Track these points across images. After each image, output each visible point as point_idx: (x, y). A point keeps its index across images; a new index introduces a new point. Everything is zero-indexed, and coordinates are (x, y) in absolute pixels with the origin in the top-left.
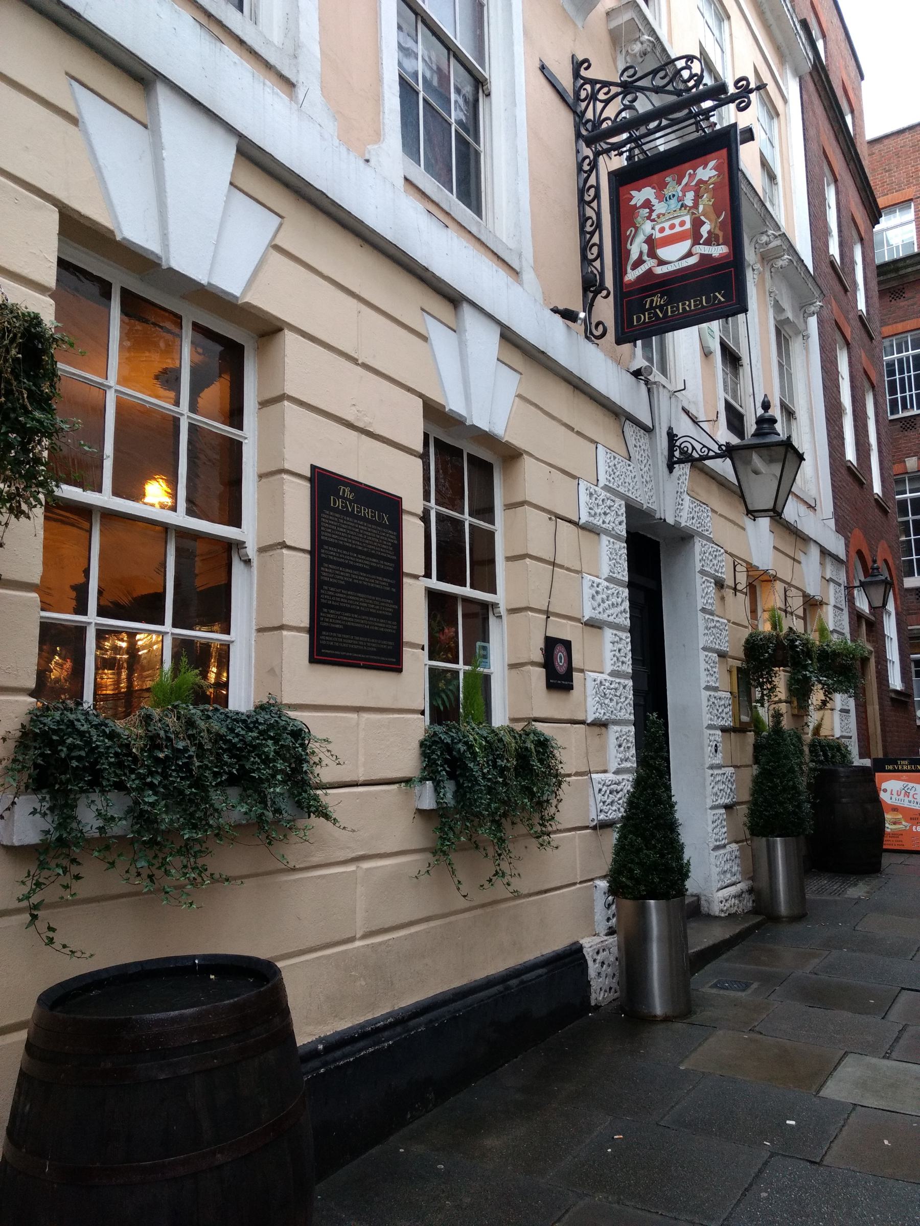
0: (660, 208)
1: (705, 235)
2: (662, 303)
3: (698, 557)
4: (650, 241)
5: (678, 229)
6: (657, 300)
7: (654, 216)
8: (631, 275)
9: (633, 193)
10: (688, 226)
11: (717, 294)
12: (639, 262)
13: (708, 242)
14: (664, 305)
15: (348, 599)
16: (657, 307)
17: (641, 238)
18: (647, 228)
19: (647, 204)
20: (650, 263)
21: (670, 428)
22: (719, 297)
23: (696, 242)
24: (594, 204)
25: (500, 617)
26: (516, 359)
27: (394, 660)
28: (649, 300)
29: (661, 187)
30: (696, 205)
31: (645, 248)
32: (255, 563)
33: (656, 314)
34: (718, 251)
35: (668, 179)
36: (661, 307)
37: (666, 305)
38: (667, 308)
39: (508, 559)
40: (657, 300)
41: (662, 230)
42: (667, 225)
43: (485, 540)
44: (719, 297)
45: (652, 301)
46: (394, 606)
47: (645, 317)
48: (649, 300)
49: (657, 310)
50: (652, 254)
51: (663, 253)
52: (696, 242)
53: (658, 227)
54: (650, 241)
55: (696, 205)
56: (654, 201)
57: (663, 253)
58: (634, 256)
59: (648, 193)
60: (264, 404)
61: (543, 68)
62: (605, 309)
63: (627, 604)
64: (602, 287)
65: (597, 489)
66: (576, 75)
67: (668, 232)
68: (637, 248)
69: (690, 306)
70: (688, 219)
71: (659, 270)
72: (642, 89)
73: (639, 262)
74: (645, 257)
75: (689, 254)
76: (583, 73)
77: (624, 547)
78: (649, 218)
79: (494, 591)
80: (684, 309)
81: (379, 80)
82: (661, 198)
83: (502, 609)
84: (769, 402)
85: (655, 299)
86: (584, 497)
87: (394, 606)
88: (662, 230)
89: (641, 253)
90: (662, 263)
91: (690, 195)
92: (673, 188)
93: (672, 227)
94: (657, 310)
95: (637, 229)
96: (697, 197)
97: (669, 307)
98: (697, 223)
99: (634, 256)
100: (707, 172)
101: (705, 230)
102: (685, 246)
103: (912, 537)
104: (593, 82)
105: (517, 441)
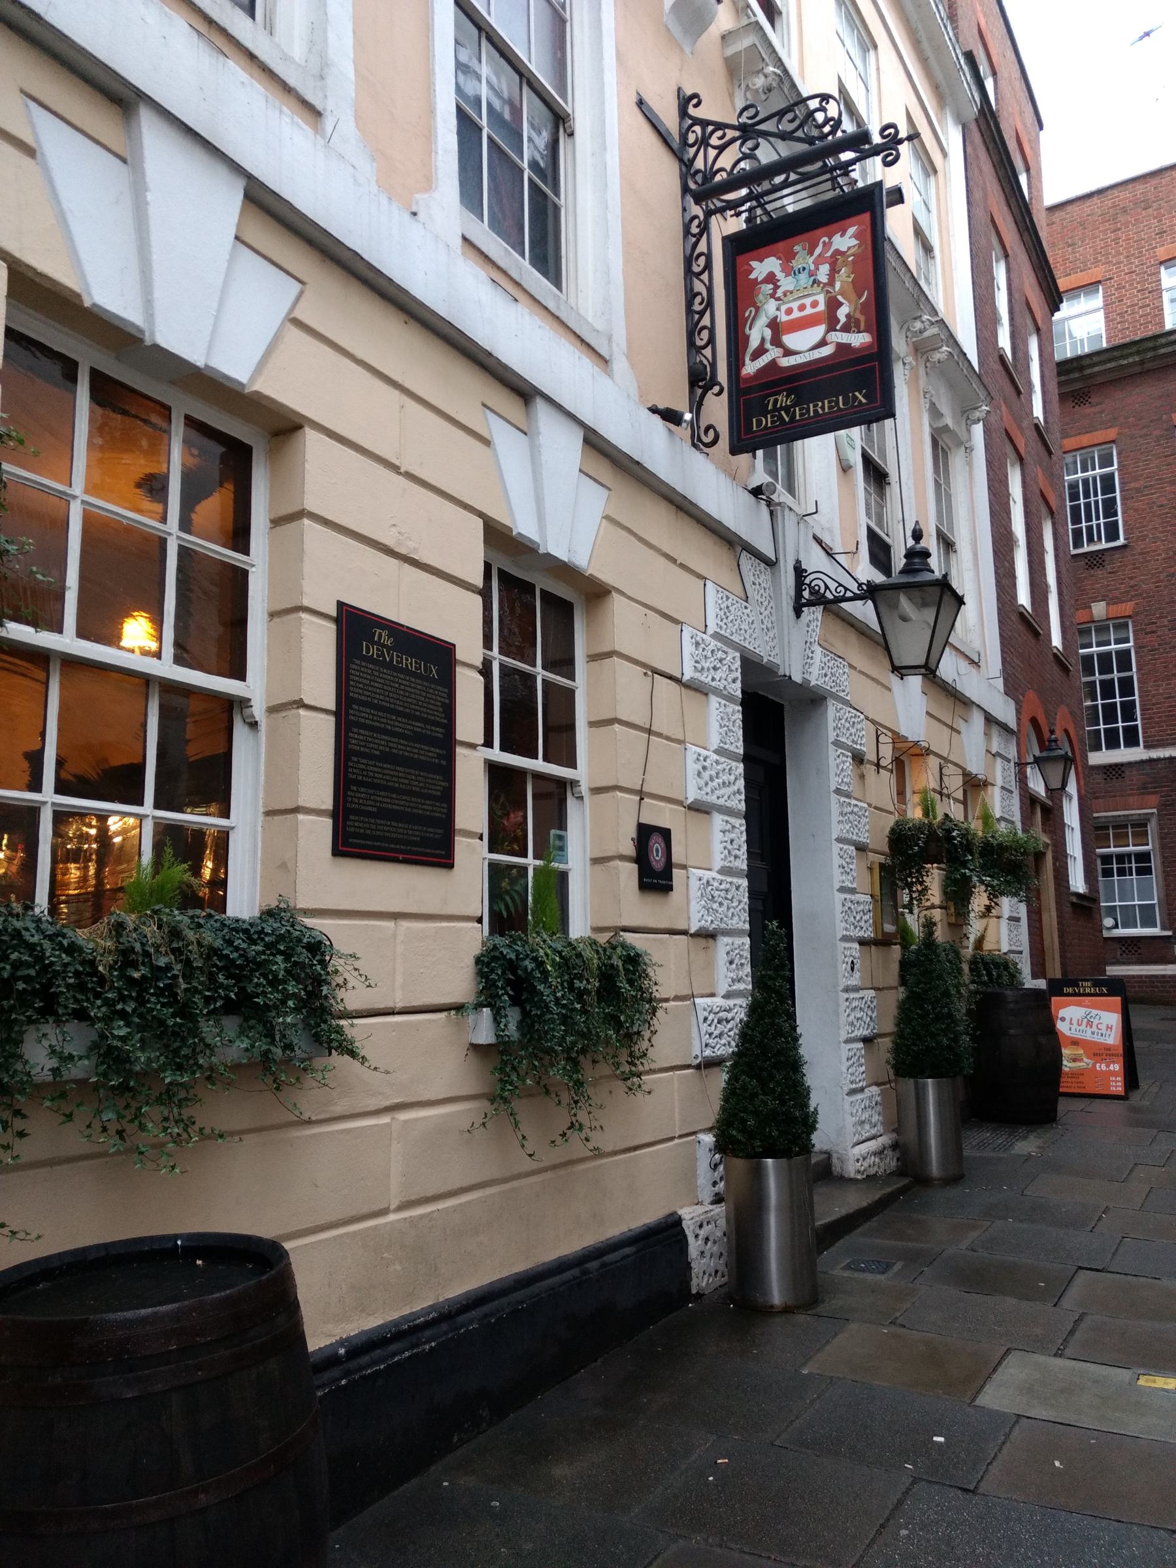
0: (787, 284)
1: (843, 320)
2: (788, 403)
3: (831, 724)
4: (774, 325)
5: (809, 311)
6: (783, 400)
7: (779, 293)
8: (750, 368)
9: (754, 264)
10: (822, 307)
11: (857, 393)
12: (760, 351)
13: (846, 329)
14: (791, 406)
15: (384, 774)
16: (782, 408)
17: (762, 321)
18: (770, 308)
19: (771, 278)
20: (773, 353)
21: (798, 562)
22: (860, 397)
23: (831, 328)
24: (705, 277)
25: (581, 798)
26: (603, 470)
27: (443, 853)
28: (772, 399)
29: (788, 257)
30: (831, 282)
31: (768, 333)
32: (263, 726)
33: (781, 418)
34: (859, 340)
35: (797, 248)
36: (787, 409)
37: (794, 405)
38: (795, 410)
39: (592, 724)
40: (783, 400)
41: (789, 311)
42: (795, 305)
43: (562, 700)
44: (860, 397)
45: (776, 401)
46: (443, 784)
47: (767, 421)
48: (772, 399)
49: (783, 413)
50: (777, 342)
51: (790, 340)
52: (831, 328)
53: (784, 308)
54: (774, 325)
55: (831, 282)
56: (780, 275)
57: (790, 340)
58: (754, 343)
59: (771, 264)
60: (277, 522)
61: (640, 103)
62: (717, 410)
63: (741, 783)
64: (713, 382)
65: (704, 636)
66: (683, 113)
67: (796, 314)
68: (757, 333)
69: (823, 408)
70: (821, 299)
71: (786, 362)
72: (765, 134)
73: (760, 351)
74: (768, 346)
75: (823, 343)
76: (692, 111)
77: (738, 711)
78: (773, 296)
79: (572, 764)
80: (816, 411)
81: (431, 111)
82: (788, 271)
83: (584, 788)
84: (921, 531)
85: (780, 398)
86: (688, 648)
87: (443, 784)
88: (789, 311)
89: (763, 340)
90: (788, 353)
91: (825, 269)
92: (803, 260)
93: (802, 308)
94: (783, 413)
95: (758, 309)
96: (834, 271)
97: (797, 409)
98: (833, 305)
99: (754, 343)
100: (846, 241)
101: (842, 313)
102: (818, 332)
103: (1100, 702)
104: (704, 123)
105: (605, 575)
